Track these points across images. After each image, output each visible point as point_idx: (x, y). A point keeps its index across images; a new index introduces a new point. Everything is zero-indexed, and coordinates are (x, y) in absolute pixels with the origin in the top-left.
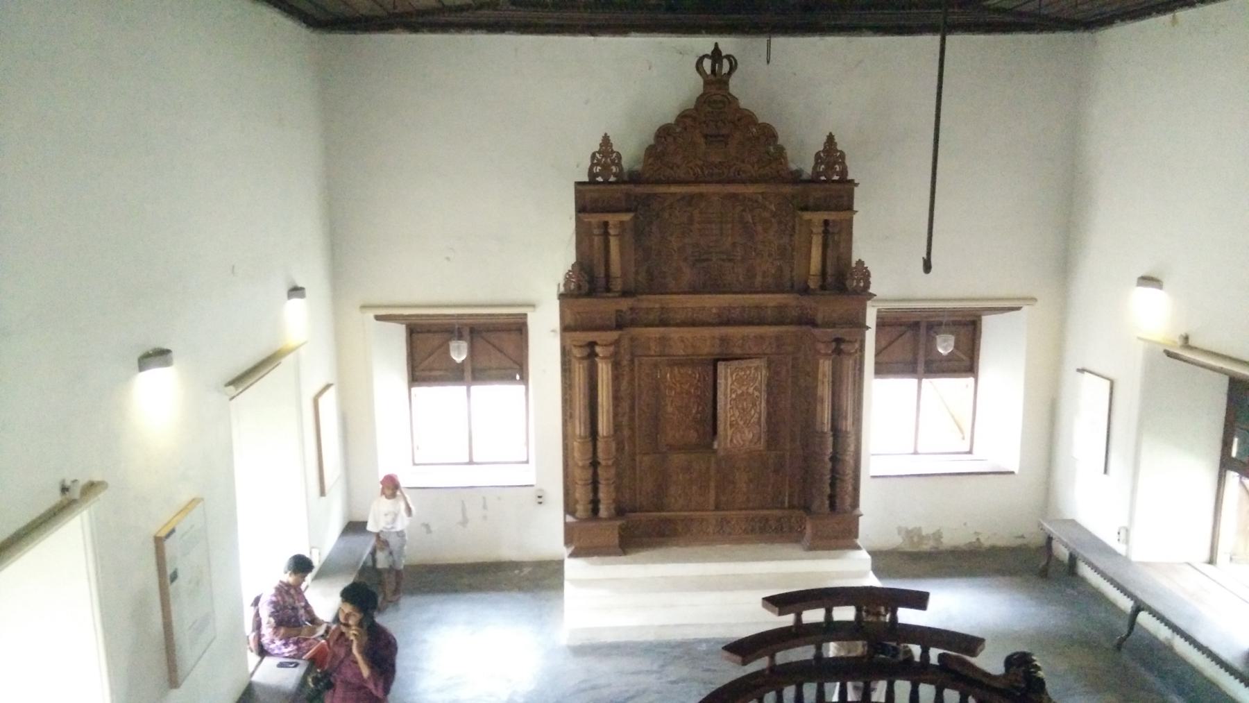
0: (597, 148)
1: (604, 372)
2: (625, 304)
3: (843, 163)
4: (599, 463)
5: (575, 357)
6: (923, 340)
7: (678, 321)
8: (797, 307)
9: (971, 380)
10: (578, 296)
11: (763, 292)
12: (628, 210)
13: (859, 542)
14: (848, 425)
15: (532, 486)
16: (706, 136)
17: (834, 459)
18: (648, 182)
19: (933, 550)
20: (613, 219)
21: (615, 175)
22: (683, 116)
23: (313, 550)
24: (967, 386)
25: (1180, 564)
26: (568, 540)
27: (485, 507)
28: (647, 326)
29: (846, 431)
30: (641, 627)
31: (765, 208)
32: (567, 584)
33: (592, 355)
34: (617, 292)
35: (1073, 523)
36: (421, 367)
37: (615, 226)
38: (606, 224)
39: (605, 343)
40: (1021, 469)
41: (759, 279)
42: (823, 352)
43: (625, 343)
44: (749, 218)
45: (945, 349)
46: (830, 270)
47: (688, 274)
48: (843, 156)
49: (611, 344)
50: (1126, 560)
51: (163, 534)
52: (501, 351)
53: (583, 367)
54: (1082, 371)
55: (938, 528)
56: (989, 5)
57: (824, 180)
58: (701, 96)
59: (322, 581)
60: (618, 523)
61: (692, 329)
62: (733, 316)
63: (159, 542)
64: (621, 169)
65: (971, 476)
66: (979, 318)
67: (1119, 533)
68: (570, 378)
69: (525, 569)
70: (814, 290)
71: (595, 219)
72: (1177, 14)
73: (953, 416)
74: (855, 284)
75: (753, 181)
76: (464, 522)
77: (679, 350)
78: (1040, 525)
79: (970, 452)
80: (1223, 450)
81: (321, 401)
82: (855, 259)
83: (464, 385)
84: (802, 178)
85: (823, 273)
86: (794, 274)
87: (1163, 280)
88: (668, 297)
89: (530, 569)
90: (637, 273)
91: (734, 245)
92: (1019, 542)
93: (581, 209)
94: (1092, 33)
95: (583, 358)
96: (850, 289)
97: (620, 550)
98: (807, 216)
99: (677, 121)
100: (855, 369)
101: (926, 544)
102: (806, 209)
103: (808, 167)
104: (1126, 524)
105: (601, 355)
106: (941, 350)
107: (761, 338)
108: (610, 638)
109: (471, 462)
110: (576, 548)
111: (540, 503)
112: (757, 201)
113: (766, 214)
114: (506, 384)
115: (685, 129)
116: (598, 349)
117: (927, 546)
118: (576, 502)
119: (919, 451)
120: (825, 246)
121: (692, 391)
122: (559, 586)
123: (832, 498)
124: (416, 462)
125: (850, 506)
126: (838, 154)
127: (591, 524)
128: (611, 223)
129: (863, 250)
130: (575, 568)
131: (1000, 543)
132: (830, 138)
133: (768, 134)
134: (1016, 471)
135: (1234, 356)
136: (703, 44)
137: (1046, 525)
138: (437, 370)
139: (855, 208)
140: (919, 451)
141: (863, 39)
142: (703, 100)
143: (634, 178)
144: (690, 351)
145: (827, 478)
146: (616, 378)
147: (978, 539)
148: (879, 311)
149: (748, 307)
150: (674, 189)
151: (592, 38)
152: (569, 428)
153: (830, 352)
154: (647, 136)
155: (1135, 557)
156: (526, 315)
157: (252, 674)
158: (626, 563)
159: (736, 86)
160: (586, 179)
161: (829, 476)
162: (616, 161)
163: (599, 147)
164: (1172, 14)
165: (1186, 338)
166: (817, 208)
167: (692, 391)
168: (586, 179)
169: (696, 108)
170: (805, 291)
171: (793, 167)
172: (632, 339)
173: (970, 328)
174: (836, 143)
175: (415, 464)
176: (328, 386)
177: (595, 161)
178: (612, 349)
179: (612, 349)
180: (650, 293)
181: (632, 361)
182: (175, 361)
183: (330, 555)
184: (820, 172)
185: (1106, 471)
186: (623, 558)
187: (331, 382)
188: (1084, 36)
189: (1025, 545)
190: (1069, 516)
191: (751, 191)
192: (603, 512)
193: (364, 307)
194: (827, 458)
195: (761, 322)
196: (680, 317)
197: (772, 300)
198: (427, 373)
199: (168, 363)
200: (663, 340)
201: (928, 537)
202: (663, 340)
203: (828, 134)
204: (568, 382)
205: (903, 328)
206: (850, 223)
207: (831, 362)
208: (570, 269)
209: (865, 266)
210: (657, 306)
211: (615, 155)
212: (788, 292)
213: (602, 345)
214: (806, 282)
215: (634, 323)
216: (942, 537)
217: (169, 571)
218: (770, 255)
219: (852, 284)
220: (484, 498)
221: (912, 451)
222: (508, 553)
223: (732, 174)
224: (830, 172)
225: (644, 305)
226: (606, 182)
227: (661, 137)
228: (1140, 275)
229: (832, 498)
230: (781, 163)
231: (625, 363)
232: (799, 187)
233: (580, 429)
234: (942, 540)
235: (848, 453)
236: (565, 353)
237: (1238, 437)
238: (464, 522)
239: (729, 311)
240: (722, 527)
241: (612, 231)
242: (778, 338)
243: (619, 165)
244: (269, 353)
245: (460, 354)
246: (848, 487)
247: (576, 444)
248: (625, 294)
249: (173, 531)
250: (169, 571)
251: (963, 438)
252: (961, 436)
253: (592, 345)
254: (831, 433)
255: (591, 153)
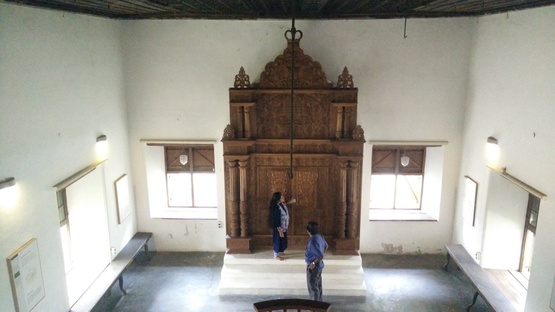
0: (238, 73)
1: (243, 173)
2: (251, 143)
3: (351, 81)
4: (241, 213)
5: (230, 166)
6: (398, 157)
7: (277, 151)
8: (331, 145)
9: (421, 176)
10: (230, 140)
11: (314, 139)
12: (252, 101)
13: (359, 252)
14: (354, 199)
15: (217, 219)
16: (288, 67)
17: (347, 214)
18: (261, 89)
19: (398, 254)
20: (246, 105)
21: (246, 85)
22: (278, 59)
23: (112, 248)
24: (419, 179)
25: (504, 270)
26: (228, 246)
27: (196, 228)
28: (262, 153)
29: (353, 203)
30: (252, 289)
31: (316, 100)
32: (224, 266)
33: (237, 165)
34: (248, 138)
35: (461, 247)
36: (171, 165)
37: (247, 108)
38: (243, 107)
39: (242, 160)
40: (439, 220)
41: (313, 132)
42: (342, 166)
43: (253, 160)
44: (309, 105)
45: (405, 164)
46: (346, 129)
47: (281, 130)
48: (351, 77)
49: (245, 161)
50: (479, 266)
51: (10, 258)
52: (206, 159)
53: (233, 171)
54: (467, 177)
55: (400, 244)
56: (415, 10)
57: (342, 88)
58: (287, 49)
59: (116, 261)
60: (249, 240)
61: (283, 155)
62: (302, 149)
63: (9, 261)
64: (249, 82)
65: (413, 222)
66: (425, 149)
67: (476, 255)
68: (228, 175)
69: (212, 256)
70: (338, 138)
71: (238, 105)
72: (508, 13)
73: (413, 192)
74: (357, 136)
75: (309, 88)
76: (187, 234)
77: (277, 164)
78: (445, 246)
79: (420, 209)
80: (526, 220)
81: (118, 184)
82: (358, 125)
83: (189, 173)
84: (333, 87)
85: (343, 131)
86: (330, 130)
87: (498, 140)
88: (272, 140)
89: (214, 256)
90: (258, 129)
91: (302, 117)
92: (439, 252)
93: (232, 101)
94: (477, 17)
95: (232, 167)
96: (354, 138)
97: (250, 251)
98: (335, 105)
99: (275, 60)
100: (358, 174)
101: (395, 251)
102: (334, 101)
103: (336, 80)
104: (479, 250)
105: (241, 166)
106: (403, 164)
107: (314, 159)
108: (238, 293)
109: (193, 207)
110: (230, 250)
111: (220, 227)
112: (312, 97)
113: (317, 103)
114: (206, 173)
115: (279, 64)
116: (239, 163)
117: (395, 252)
118: (231, 229)
119: (396, 208)
120: (343, 118)
121: (283, 182)
122: (221, 265)
123: (346, 231)
124: (170, 206)
125: (355, 235)
126: (349, 77)
127: (237, 240)
128: (245, 107)
129: (362, 120)
130: (228, 258)
131: (430, 252)
132: (346, 69)
133: (317, 66)
134: (438, 220)
135: (522, 180)
136: (287, 23)
137: (448, 248)
138: (178, 166)
139: (358, 102)
140: (396, 208)
141: (365, 20)
142: (286, 51)
143: (256, 86)
144: (282, 164)
145: (344, 222)
146: (248, 176)
147: (419, 250)
148: (374, 146)
149: (309, 145)
150: (273, 92)
151: (241, 21)
152: (228, 197)
153: (345, 166)
154: (260, 69)
155: (484, 266)
156: (213, 144)
157: (71, 309)
158: (251, 258)
159: (302, 45)
160: (233, 87)
161: (345, 222)
162: (247, 79)
163: (239, 73)
164: (507, 13)
165: (505, 169)
166: (339, 102)
167: (283, 182)
168: (233, 87)
169: (284, 54)
170: (334, 139)
171: (329, 82)
172: (256, 158)
173: (421, 152)
174: (348, 71)
175: (169, 207)
176: (124, 175)
177: (237, 79)
178: (246, 163)
179: (246, 163)
180: (263, 138)
181: (256, 168)
182: (107, 139)
183: (125, 247)
184: (341, 85)
185: (473, 225)
186: (253, 255)
187: (125, 173)
188: (474, 19)
189: (441, 253)
190: (460, 243)
191: (310, 93)
192: (243, 234)
193: (141, 140)
194: (344, 214)
195: (315, 152)
196: (278, 149)
197: (320, 142)
198: (174, 167)
199: (105, 139)
200: (269, 159)
201: (396, 248)
202: (269, 159)
203: (344, 67)
204: (228, 177)
205: (387, 152)
206: (356, 107)
207: (346, 171)
208: (226, 127)
209: (361, 128)
210: (267, 144)
211: (246, 76)
212: (326, 139)
213: (241, 161)
214: (335, 134)
215: (256, 152)
216: (402, 249)
217: (14, 272)
218: (319, 121)
219: (354, 136)
220: (196, 224)
221: (393, 208)
222: (205, 248)
223: (300, 85)
224: (345, 85)
225: (261, 143)
226: (242, 89)
227: (268, 68)
228: (489, 136)
229: (346, 231)
230: (323, 80)
231: (253, 169)
232: (331, 91)
233: (232, 198)
234: (403, 250)
235: (354, 212)
236: (225, 163)
237: (533, 214)
238: (187, 234)
239: (299, 146)
240: (297, 242)
241: (245, 111)
242: (322, 159)
243: (248, 81)
244: (86, 165)
245: (184, 161)
246: (353, 228)
247: (230, 204)
248: (253, 138)
249: (17, 255)
250: (14, 272)
251: (417, 202)
252: (416, 201)
253: (237, 161)
254: (346, 203)
255: (235, 76)
